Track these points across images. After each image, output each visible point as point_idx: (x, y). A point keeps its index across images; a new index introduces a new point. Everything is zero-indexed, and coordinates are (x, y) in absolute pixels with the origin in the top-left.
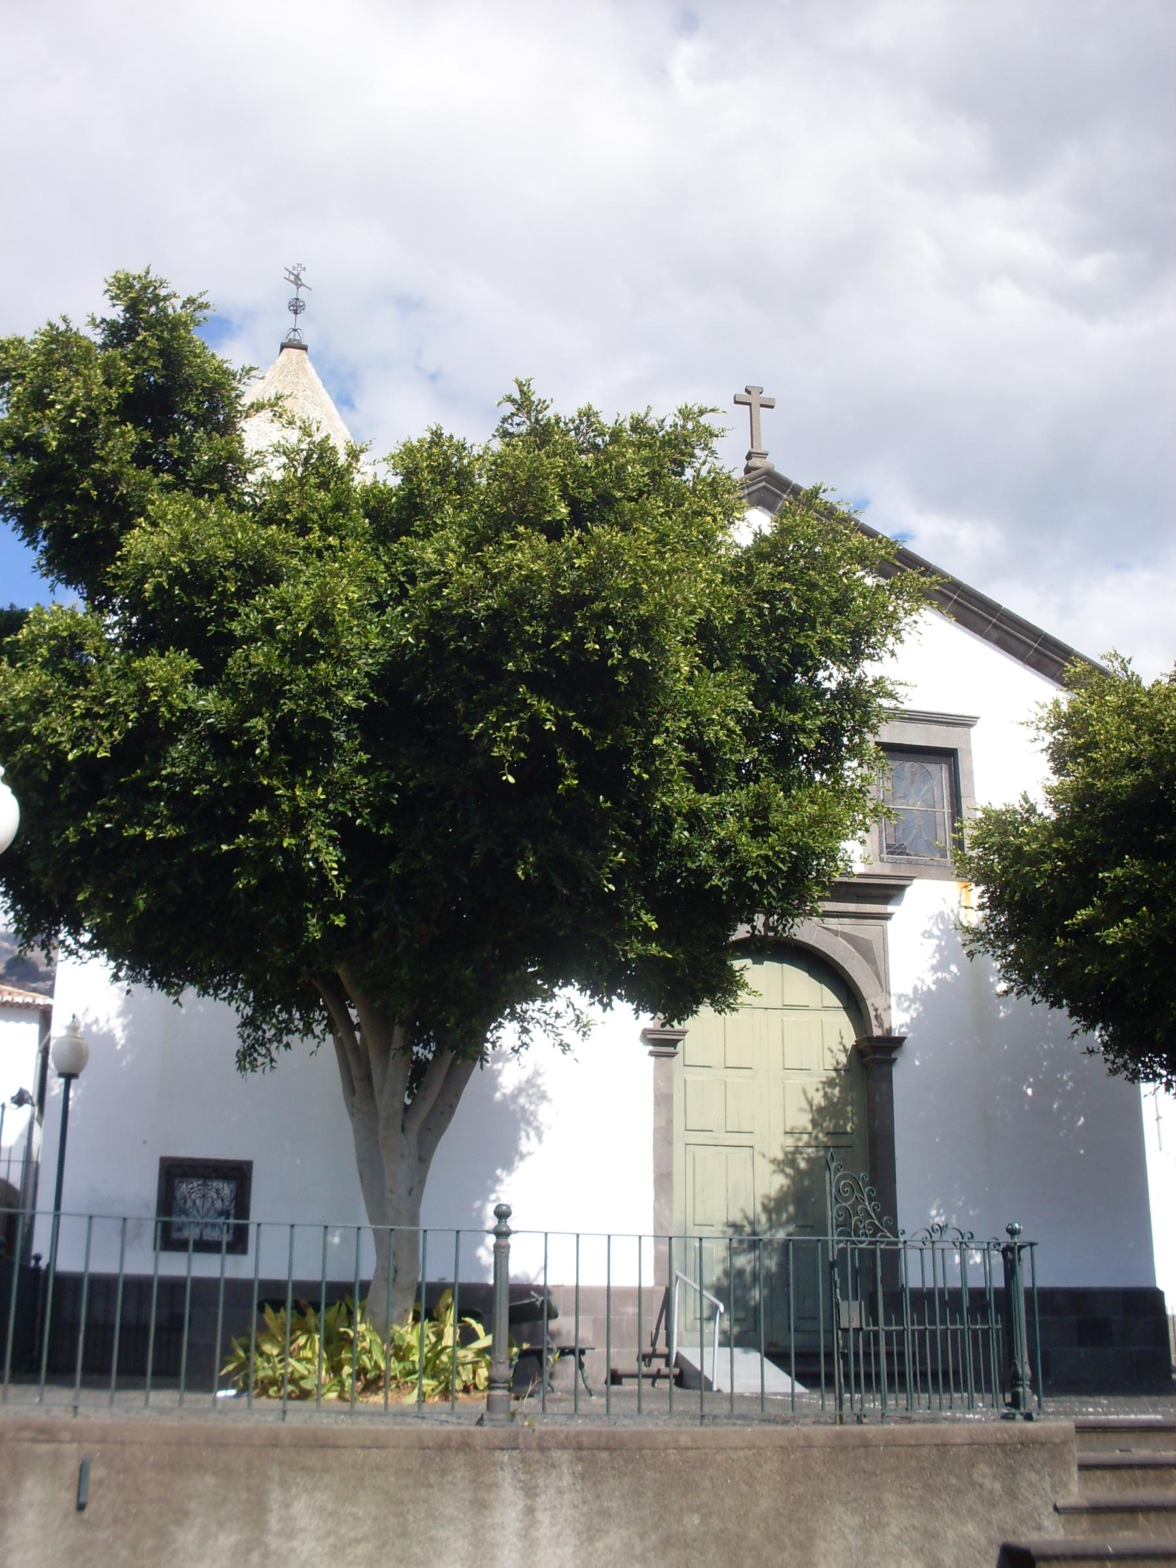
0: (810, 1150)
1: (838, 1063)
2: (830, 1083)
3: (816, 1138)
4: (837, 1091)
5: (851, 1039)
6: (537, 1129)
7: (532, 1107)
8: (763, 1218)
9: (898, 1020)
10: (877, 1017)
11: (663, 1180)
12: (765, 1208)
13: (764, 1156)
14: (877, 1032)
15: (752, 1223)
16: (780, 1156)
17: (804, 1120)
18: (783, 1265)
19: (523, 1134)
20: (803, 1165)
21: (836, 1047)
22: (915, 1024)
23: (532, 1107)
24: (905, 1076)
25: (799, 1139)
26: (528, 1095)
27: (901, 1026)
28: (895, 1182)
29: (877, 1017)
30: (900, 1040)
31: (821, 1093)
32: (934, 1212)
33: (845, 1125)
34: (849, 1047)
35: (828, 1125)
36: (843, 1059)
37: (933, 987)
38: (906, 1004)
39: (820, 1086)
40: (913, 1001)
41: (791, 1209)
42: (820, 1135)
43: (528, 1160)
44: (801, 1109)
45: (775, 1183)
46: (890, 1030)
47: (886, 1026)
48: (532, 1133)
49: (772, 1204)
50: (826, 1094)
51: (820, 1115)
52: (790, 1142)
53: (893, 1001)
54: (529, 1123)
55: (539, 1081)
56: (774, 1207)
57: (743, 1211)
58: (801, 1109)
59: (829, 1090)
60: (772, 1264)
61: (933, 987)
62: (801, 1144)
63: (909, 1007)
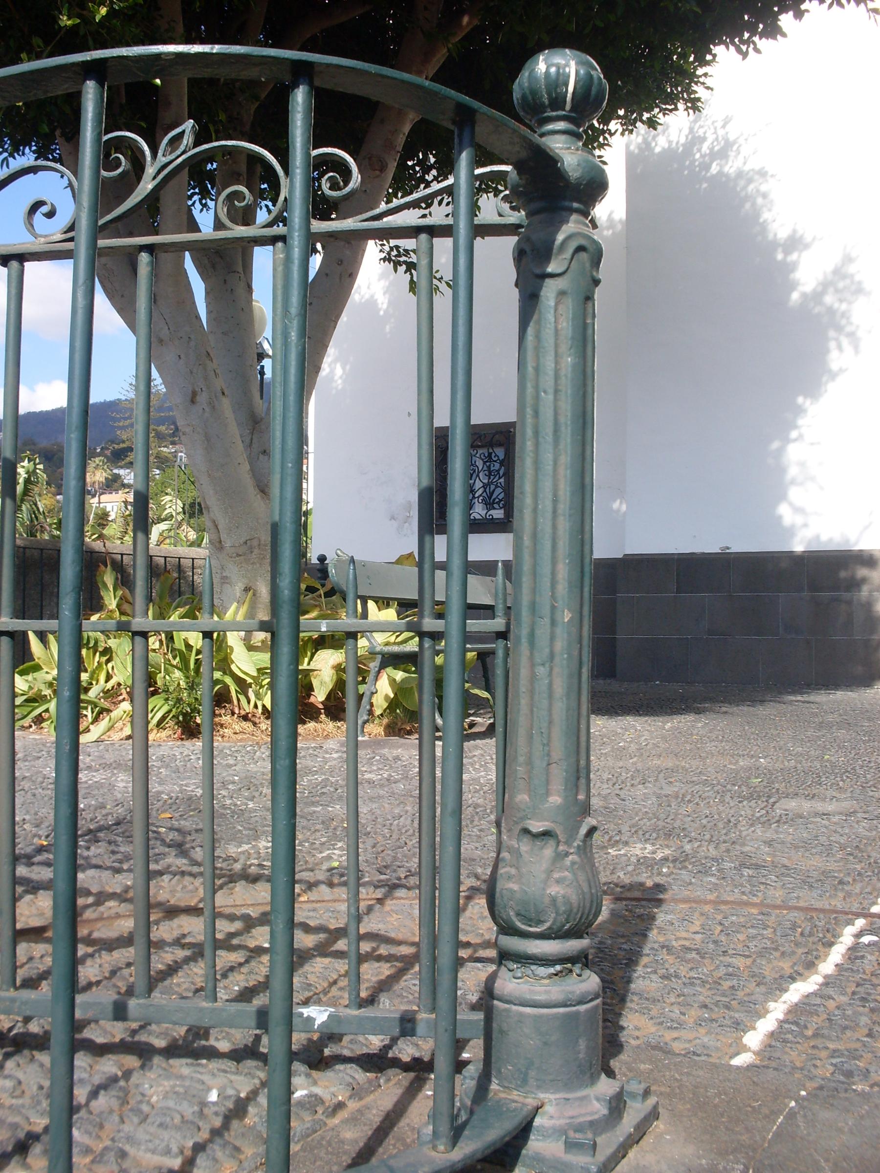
6: (851, 335)
7: (844, 307)
19: (832, 345)
23: (844, 307)
26: (837, 291)
43: (840, 379)
48: (845, 342)
54: (839, 329)
55: (852, 269)
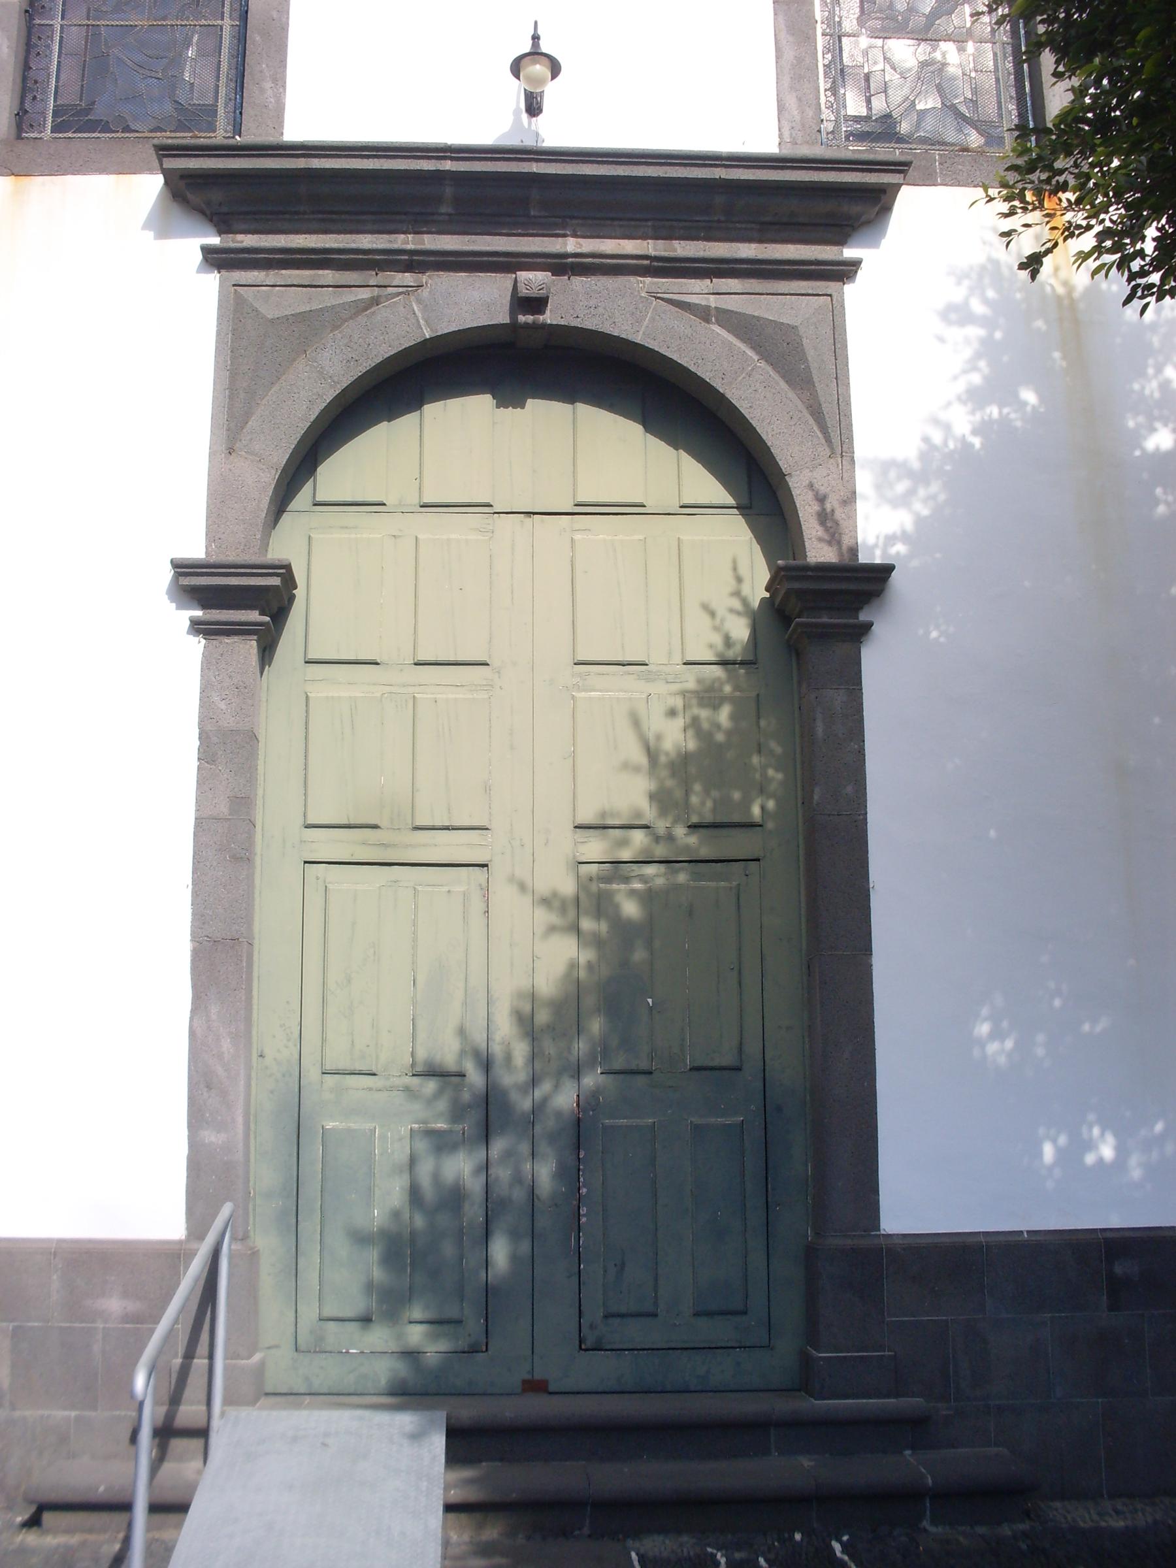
0: (650, 870)
1: (728, 642)
2: (708, 696)
3: (670, 838)
4: (724, 715)
5: (757, 581)
8: (520, 1051)
9: (878, 526)
10: (824, 517)
11: (222, 955)
12: (526, 1024)
13: (522, 887)
14: (819, 552)
15: (486, 1064)
16: (567, 887)
17: (633, 794)
18: (570, 1174)
20: (630, 909)
21: (723, 602)
22: (915, 539)
24: (891, 668)
25: (624, 843)
27: (891, 539)
28: (868, 950)
29: (824, 517)
30: (885, 571)
31: (679, 722)
32: (984, 1029)
33: (746, 804)
34: (756, 604)
35: (702, 804)
36: (741, 631)
37: (977, 442)
38: (901, 487)
39: (679, 702)
40: (920, 477)
41: (596, 1026)
42: (680, 831)
44: (626, 766)
45: (552, 960)
46: (854, 551)
47: (847, 541)
49: (543, 1017)
50: (695, 723)
51: (676, 776)
52: (595, 848)
53: (864, 481)
56: (548, 1025)
57: (462, 1032)
58: (626, 766)
59: (704, 714)
60: (545, 1173)
61: (977, 442)
62: (626, 855)
63: (911, 492)
